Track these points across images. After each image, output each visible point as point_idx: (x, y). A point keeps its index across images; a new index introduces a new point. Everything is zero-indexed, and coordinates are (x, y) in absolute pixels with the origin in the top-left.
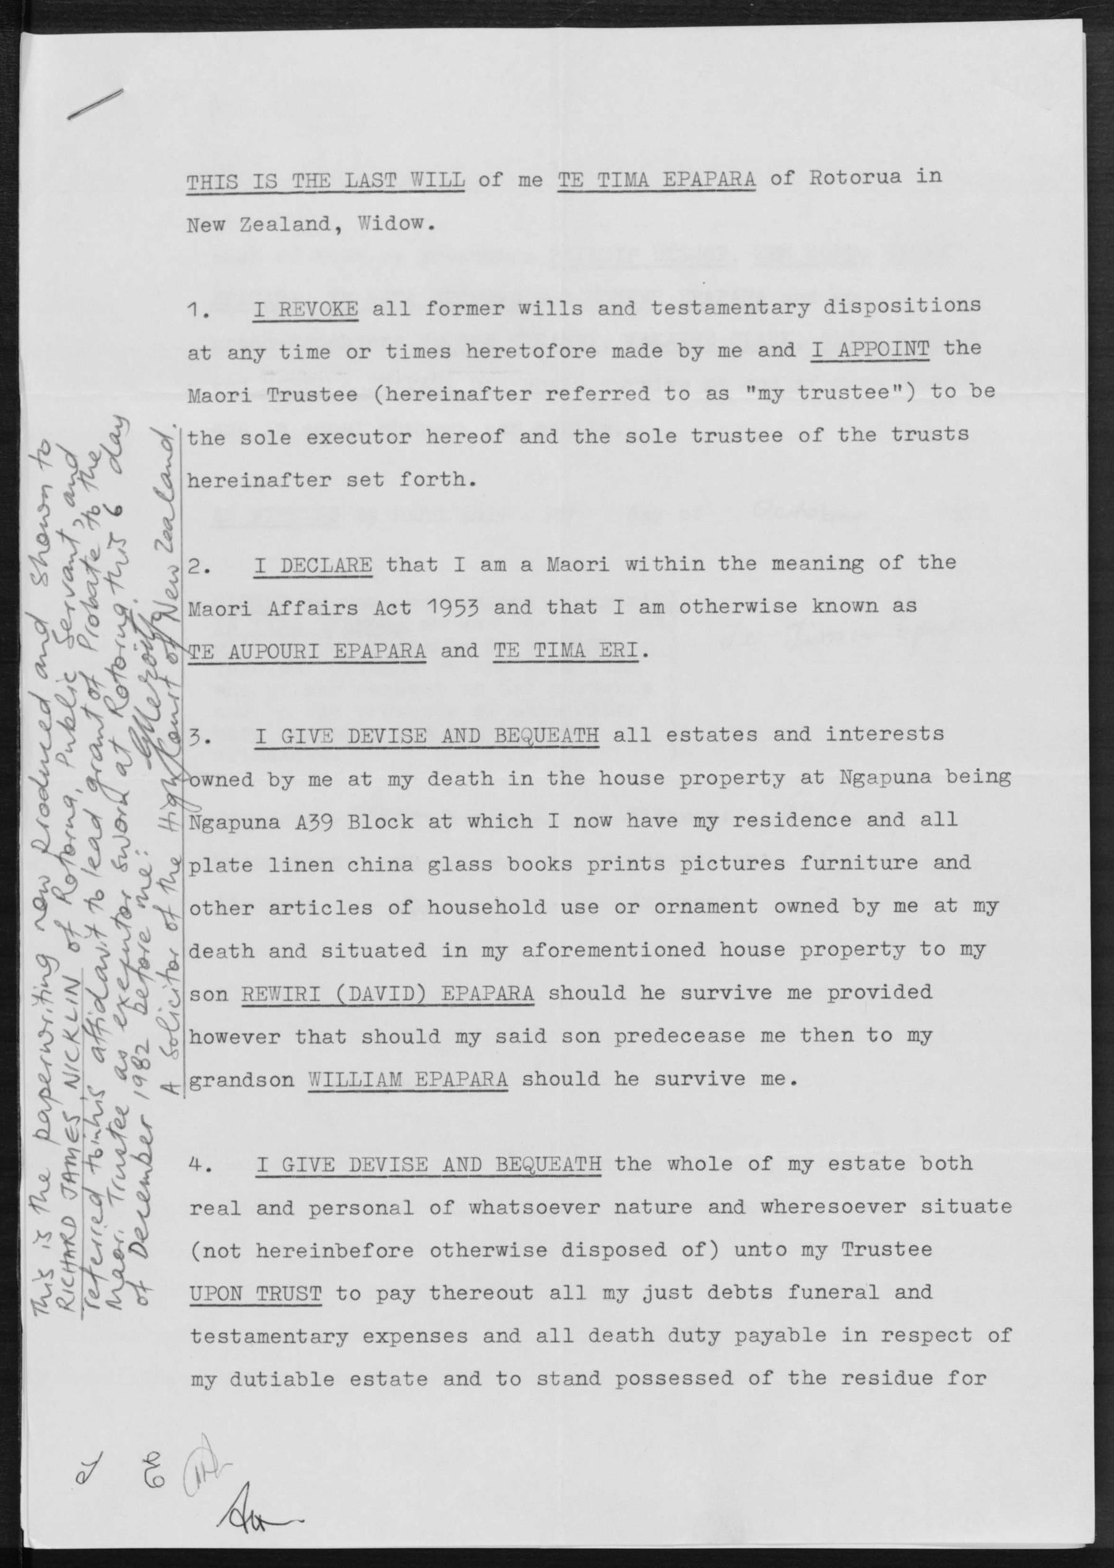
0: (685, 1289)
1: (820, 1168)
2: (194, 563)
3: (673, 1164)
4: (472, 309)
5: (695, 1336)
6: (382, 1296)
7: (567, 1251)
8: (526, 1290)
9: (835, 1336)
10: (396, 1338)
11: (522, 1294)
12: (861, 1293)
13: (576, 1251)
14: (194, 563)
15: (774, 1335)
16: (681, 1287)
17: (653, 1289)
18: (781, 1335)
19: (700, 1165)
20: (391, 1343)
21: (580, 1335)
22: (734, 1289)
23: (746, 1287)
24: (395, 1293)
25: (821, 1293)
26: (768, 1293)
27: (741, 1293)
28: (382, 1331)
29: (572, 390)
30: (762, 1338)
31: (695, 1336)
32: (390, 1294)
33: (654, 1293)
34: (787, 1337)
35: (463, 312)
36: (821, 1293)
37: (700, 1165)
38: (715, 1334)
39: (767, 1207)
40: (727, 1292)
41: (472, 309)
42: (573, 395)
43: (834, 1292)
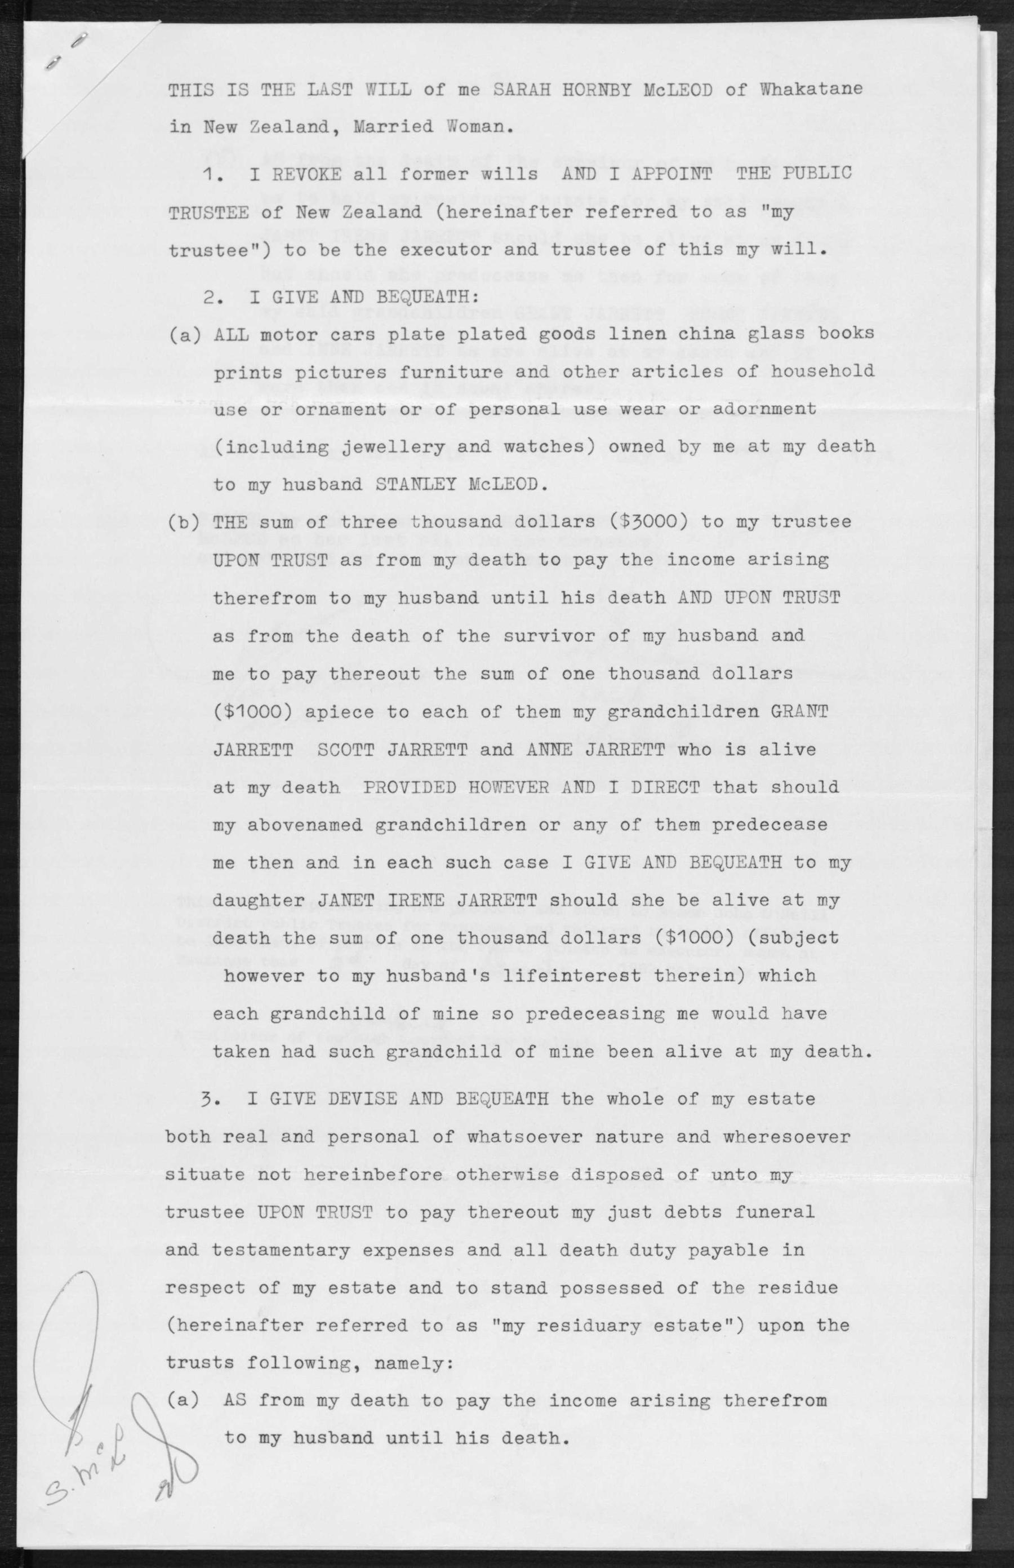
0: (645, 1209)
1: (740, 1102)
2: (209, 294)
3: (612, 1099)
4: (440, 175)
5: (654, 1251)
6: (426, 1214)
7: (576, 1176)
8: (553, 1210)
9: (776, 1250)
10: (392, 1251)
11: (549, 1213)
12: (799, 1213)
13: (584, 1176)
14: (209, 294)
15: (722, 1250)
16: (641, 1208)
17: (617, 1209)
18: (729, 1250)
19: (635, 1100)
20: (387, 1256)
21: (553, 1249)
22: (688, 1210)
23: (699, 1208)
24: (437, 1214)
25: (763, 1213)
26: (717, 1213)
27: (694, 1213)
28: (379, 1246)
29: (609, 208)
30: (712, 1252)
31: (654, 1251)
32: (432, 1213)
33: (618, 1213)
34: (734, 1250)
35: (433, 177)
36: (763, 1213)
37: (635, 1100)
38: (671, 1250)
39: (729, 1138)
40: (682, 1212)
41: (440, 175)
42: (610, 213)
43: (775, 1212)
